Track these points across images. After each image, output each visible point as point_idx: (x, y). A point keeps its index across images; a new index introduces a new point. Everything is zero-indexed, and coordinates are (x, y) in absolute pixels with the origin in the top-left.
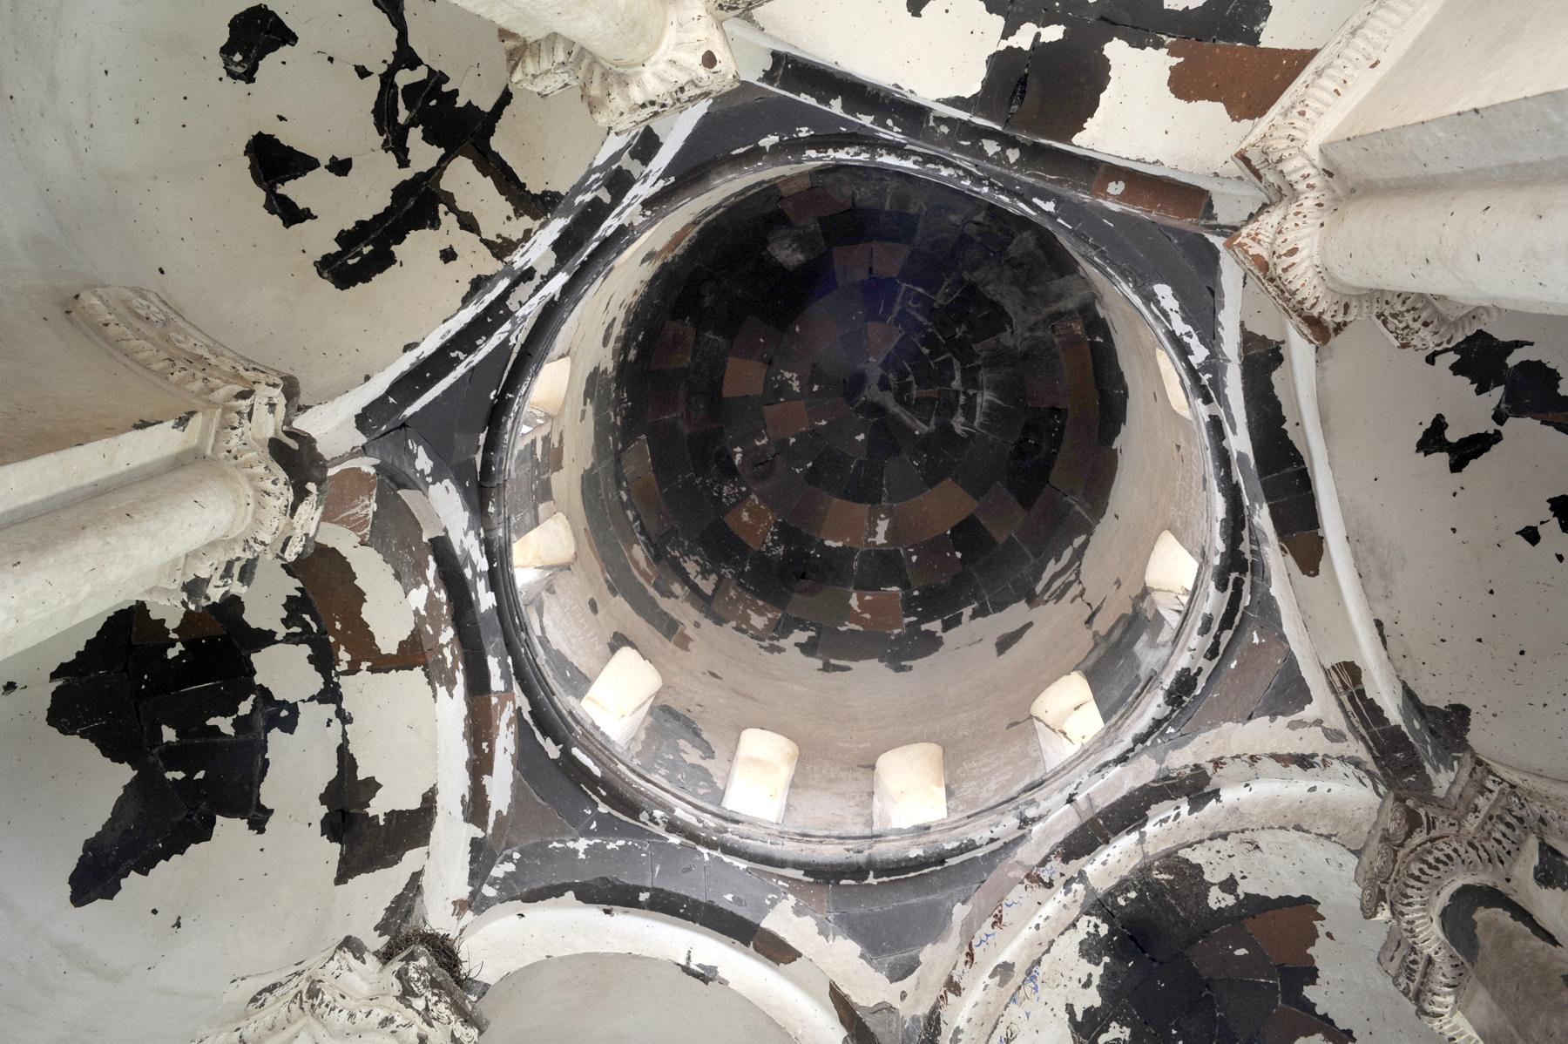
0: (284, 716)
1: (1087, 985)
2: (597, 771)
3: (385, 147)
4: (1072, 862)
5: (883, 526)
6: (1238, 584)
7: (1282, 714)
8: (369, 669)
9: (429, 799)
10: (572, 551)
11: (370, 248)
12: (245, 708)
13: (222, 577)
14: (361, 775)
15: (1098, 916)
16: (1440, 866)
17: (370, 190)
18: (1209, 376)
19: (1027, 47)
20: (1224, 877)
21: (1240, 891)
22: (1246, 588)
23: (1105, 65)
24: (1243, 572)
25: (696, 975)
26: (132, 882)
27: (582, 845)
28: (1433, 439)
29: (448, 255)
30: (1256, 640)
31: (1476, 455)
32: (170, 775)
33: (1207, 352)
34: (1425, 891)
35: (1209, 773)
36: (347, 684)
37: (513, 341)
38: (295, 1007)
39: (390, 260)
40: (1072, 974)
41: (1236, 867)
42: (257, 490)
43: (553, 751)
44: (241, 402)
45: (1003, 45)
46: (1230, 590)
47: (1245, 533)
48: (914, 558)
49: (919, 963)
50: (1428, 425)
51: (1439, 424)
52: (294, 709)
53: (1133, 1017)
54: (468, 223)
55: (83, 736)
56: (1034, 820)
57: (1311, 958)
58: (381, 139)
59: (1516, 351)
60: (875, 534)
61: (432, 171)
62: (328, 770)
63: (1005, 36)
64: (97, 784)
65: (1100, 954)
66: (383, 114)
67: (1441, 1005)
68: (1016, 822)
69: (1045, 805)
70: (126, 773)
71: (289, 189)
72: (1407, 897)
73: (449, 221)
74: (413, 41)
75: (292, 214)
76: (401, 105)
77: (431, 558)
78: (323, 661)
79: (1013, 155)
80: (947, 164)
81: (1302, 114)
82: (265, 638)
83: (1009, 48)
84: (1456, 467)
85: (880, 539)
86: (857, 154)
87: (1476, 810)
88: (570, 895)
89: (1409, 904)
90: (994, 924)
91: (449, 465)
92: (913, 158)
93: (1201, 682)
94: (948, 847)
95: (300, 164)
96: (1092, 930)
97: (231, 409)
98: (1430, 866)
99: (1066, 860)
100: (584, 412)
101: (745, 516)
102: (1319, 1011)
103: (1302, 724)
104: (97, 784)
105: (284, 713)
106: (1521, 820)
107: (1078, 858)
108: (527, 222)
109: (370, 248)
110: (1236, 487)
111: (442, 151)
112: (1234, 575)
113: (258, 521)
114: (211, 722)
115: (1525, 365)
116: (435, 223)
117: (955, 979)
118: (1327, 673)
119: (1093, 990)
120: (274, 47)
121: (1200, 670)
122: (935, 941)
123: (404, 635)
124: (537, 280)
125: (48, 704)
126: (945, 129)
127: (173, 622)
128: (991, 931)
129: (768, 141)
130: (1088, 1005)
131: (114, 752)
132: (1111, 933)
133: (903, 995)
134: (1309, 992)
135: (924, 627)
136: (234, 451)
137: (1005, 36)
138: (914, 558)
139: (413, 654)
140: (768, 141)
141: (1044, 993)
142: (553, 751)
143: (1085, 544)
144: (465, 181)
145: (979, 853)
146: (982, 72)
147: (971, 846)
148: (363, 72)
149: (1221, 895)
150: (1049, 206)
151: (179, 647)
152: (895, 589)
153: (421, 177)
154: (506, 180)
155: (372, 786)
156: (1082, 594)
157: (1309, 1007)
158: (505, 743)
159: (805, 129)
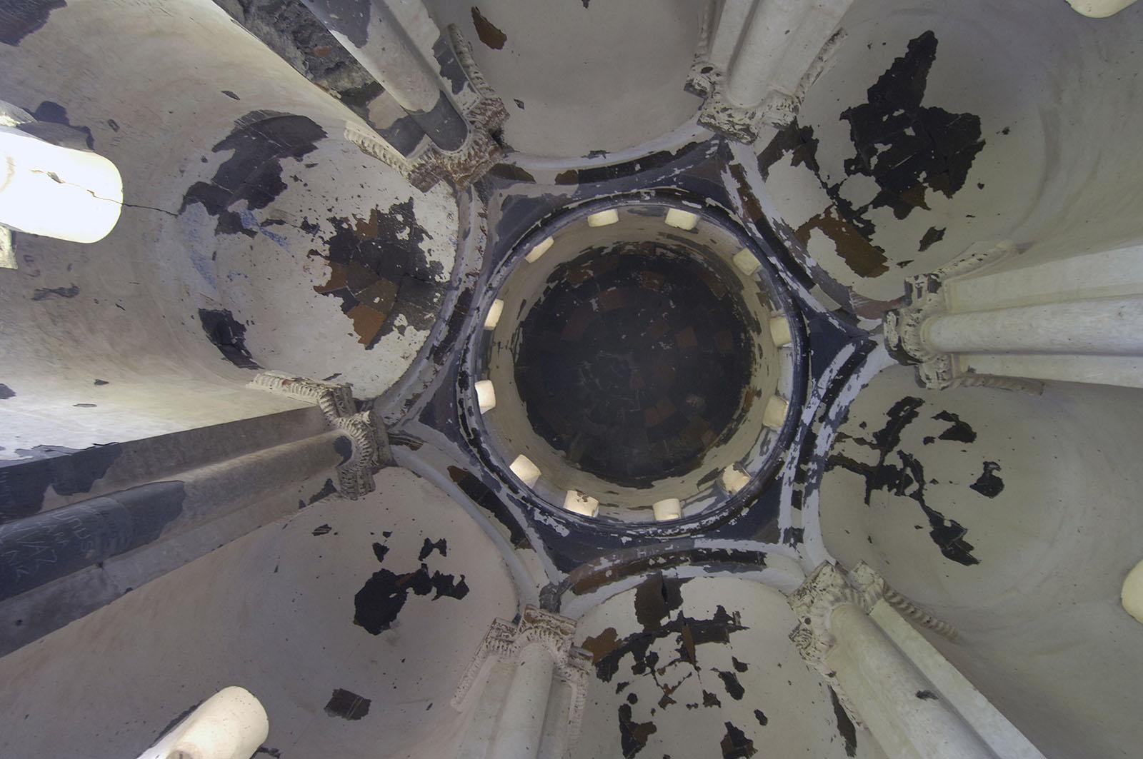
0: (853, 166)
1: (429, 251)
2: (685, 203)
3: (911, 456)
4: (464, 290)
5: (595, 307)
6: (469, 435)
7: (425, 408)
8: (820, 215)
9: (764, 173)
10: (735, 260)
11: (901, 415)
12: (874, 161)
13: (922, 288)
14: (803, 163)
16: (363, 458)
17: (910, 438)
18: (529, 509)
19: (671, 612)
20: (406, 332)
22: (465, 435)
23: (640, 621)
24: (470, 440)
25: (598, 152)
26: (902, 51)
27: (677, 172)
28: (442, 546)
29: (863, 425)
30: (449, 420)
31: (423, 549)
32: (902, 111)
33: (536, 518)
36: (828, 201)
37: (814, 380)
38: (801, 96)
39: (889, 414)
40: (439, 252)
42: (923, 349)
43: (710, 201)
44: (945, 385)
45: (680, 608)
47: (478, 456)
48: (575, 302)
50: (447, 550)
51: (443, 552)
52: (849, 172)
54: (861, 441)
55: (957, 115)
56: (487, 291)
58: (914, 458)
59: (436, 594)
60: (596, 302)
61: (886, 454)
62: (819, 156)
63: (681, 612)
64: (939, 91)
65: (432, 266)
66: (918, 468)
67: (324, 402)
68: (494, 286)
69: (487, 297)
70: (926, 103)
71: (949, 425)
73: (869, 438)
74: (917, 503)
75: (944, 416)
76: (911, 475)
77: (811, 277)
78: (844, 206)
79: (652, 562)
80: (671, 535)
81: (584, 695)
82: (877, 203)
83: (677, 608)
84: (427, 541)
85: (593, 301)
86: (707, 522)
87: (361, 478)
88: (674, 153)
89: (363, 437)
90: (481, 247)
91: (821, 319)
92: (685, 531)
93: (458, 389)
94: (515, 258)
95: (946, 436)
97: (949, 380)
98: (366, 456)
100: (756, 315)
101: (656, 281)
102: (331, 295)
104: (939, 91)
105: (853, 168)
106: (348, 493)
108: (835, 453)
109: (901, 415)
110: (493, 471)
111: (885, 464)
112: (472, 437)
113: (917, 335)
114: (889, 146)
115: (429, 591)
116: (875, 435)
117: (485, 219)
118: (423, 441)
119: (425, 250)
120: (979, 480)
122: (500, 222)
123: (810, 242)
124: (816, 419)
125: (982, 126)
126: (682, 558)
127: (929, 192)
128: (481, 244)
129: (745, 512)
130: (423, 242)
131: (937, 112)
133: (501, 195)
134: (340, 301)
135: (557, 282)
136: (940, 361)
137: (681, 612)
138: (575, 302)
139: (802, 235)
140: (745, 512)
141: (446, 240)
142: (710, 201)
143: (514, 360)
144: (870, 457)
145: (501, 263)
146: (682, 595)
147: (506, 264)
148: (934, 481)
149: (402, 323)
150: (624, 539)
151: (921, 180)
152: (576, 287)
153: (890, 450)
154: (851, 465)
155: (795, 163)
156: (506, 347)
157: (336, 294)
158: (736, 200)
159: (733, 524)
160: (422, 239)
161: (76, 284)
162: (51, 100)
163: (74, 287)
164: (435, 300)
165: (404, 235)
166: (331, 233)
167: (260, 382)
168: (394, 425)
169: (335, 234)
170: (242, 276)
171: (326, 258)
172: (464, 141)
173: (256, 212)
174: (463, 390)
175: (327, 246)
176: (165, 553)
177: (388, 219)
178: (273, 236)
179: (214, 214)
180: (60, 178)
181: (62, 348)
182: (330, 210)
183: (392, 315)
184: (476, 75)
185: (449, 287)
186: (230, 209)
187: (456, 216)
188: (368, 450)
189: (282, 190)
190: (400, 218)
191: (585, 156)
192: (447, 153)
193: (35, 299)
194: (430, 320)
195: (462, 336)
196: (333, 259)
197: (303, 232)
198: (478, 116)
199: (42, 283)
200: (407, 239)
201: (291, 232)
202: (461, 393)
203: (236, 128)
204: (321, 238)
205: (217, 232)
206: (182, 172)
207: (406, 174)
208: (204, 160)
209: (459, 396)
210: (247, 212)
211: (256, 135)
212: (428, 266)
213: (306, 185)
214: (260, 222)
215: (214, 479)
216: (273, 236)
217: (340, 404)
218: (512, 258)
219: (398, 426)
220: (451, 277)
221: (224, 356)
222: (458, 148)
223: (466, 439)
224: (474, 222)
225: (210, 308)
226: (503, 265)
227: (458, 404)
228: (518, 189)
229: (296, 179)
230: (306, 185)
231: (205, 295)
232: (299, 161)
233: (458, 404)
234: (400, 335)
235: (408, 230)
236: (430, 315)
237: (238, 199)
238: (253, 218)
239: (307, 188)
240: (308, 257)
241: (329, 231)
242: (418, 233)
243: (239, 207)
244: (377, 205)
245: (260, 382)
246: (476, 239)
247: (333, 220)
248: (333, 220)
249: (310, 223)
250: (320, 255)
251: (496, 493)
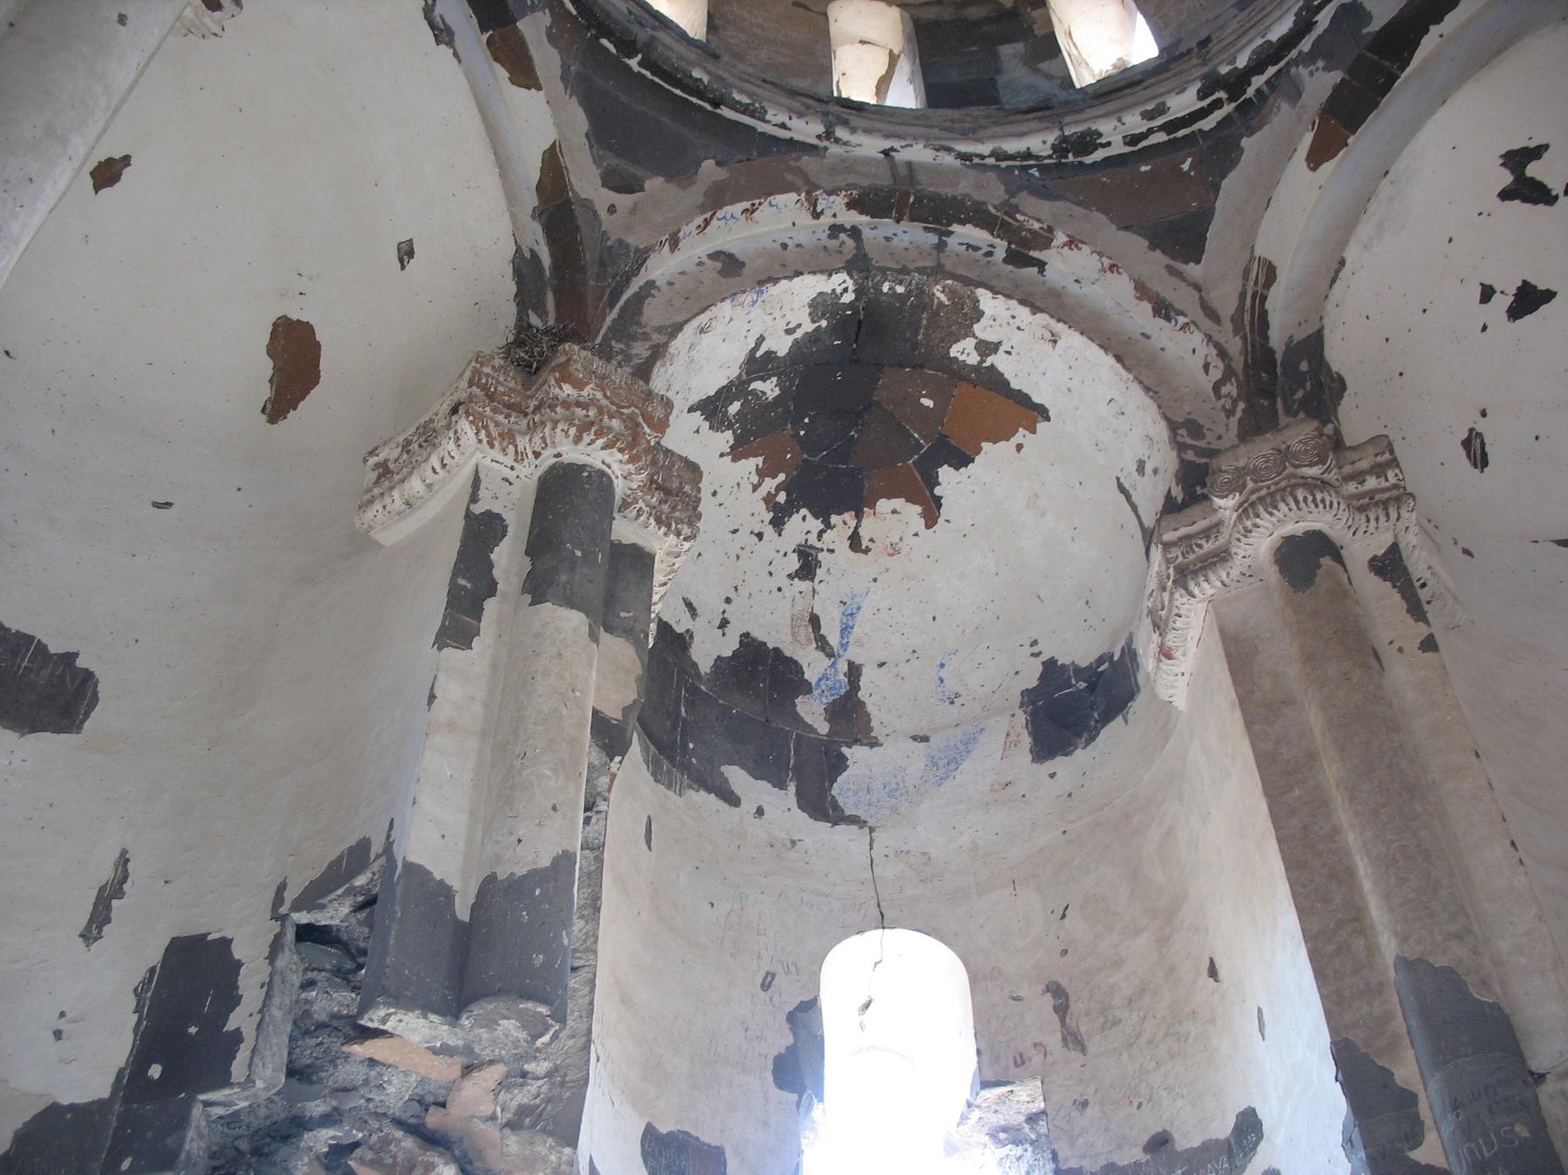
1: (789, 332)
4: (853, 212)
6: (1218, 104)
7: (1164, 252)
15: (856, 283)
21: (989, 361)
22: (1218, 115)
24: (1231, 100)
34: (1292, 514)
35: (1055, 243)
41: (1011, 339)
46: (1205, 103)
47: (1271, 71)
49: (641, 189)
50: (1532, 144)
51: (1537, 152)
53: (792, 384)
57: (978, 451)
65: (823, 315)
68: (821, 129)
72: (1276, 507)
89: (1271, 514)
90: (746, 210)
93: (1099, 155)
94: (737, 96)
96: (839, 291)
98: (1314, 501)
99: (850, 206)
102: (938, 491)
103: (1180, 276)
107: (861, 213)
112: (1222, 95)
117: (681, 235)
118: (1252, 258)
119: (790, 339)
121: (1109, 144)
128: (738, 214)
130: (774, 349)
132: (851, 305)
133: (612, 209)
134: (945, 473)
141: (757, 311)
145: (761, 127)
157: (933, 481)
160: (769, 353)
161: (1043, 987)
162: (770, 1078)
163: (1048, 990)
164: (900, 289)
165: (769, 388)
166: (804, 518)
167: (1171, 692)
168: (1222, 354)
169: (804, 511)
170: (944, 673)
171: (859, 516)
172: (584, 466)
173: (811, 675)
174: (1103, 140)
175: (834, 519)
176: (1523, 960)
177: (743, 427)
178: (846, 630)
179: (844, 759)
180: (864, 1001)
181: (1159, 1015)
182: (760, 536)
183: (957, 372)
184: (438, 469)
185: (859, 265)
186: (823, 728)
187: (702, 319)
188: (1300, 498)
189: (754, 640)
190: (735, 407)
191: (456, 55)
192: (620, 487)
193: (1083, 1050)
194: (951, 293)
195: (966, 186)
196: (858, 503)
197: (820, 573)
198: (520, 448)
199: (1054, 1040)
200: (774, 379)
201: (826, 598)
202: (1109, 144)
203: (690, 787)
204: (820, 535)
205: (874, 743)
206: (793, 842)
207: (687, 545)
208: (760, 812)
209: (1118, 148)
210: (816, 692)
211: (685, 746)
212: (824, 323)
213: (728, 601)
214: (828, 662)
215: (1387, 897)
216: (846, 630)
217: (1200, 546)
218: (739, 102)
219: (1221, 339)
220: (837, 271)
221: (1120, 718)
222: (602, 474)
223: (1228, 108)
224: (695, 248)
225: (1026, 740)
226: (763, 120)
227: (1140, 146)
228: (586, 181)
229: (724, 624)
230: (728, 601)
231: (1003, 745)
232: (691, 637)
233: (1140, 146)
234: (1002, 349)
235: (757, 385)
236: (938, 294)
237: (798, 719)
238: (825, 677)
239: (732, 595)
240: (867, 551)
241: (802, 525)
242: (759, 364)
243: (812, 711)
244: (722, 455)
245: (1171, 692)
246: (735, 230)
247: (778, 524)
248: (778, 524)
249: (797, 566)
250: (856, 528)
251: (1375, 26)
